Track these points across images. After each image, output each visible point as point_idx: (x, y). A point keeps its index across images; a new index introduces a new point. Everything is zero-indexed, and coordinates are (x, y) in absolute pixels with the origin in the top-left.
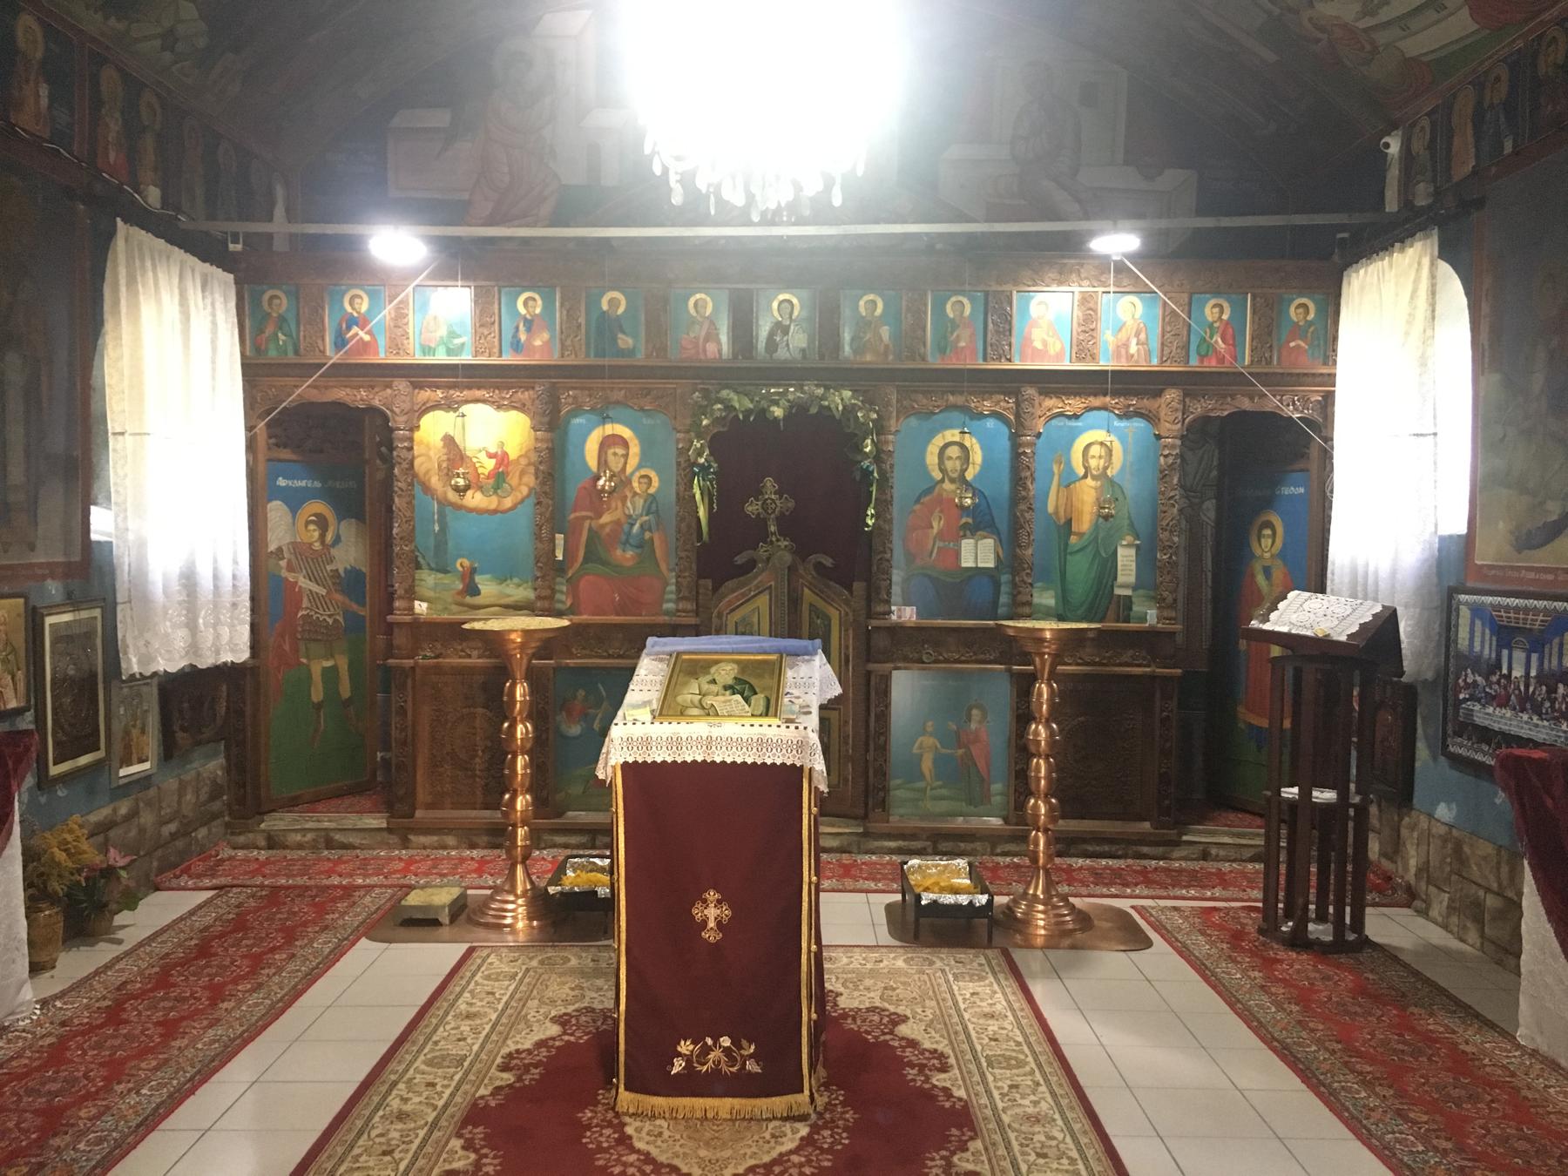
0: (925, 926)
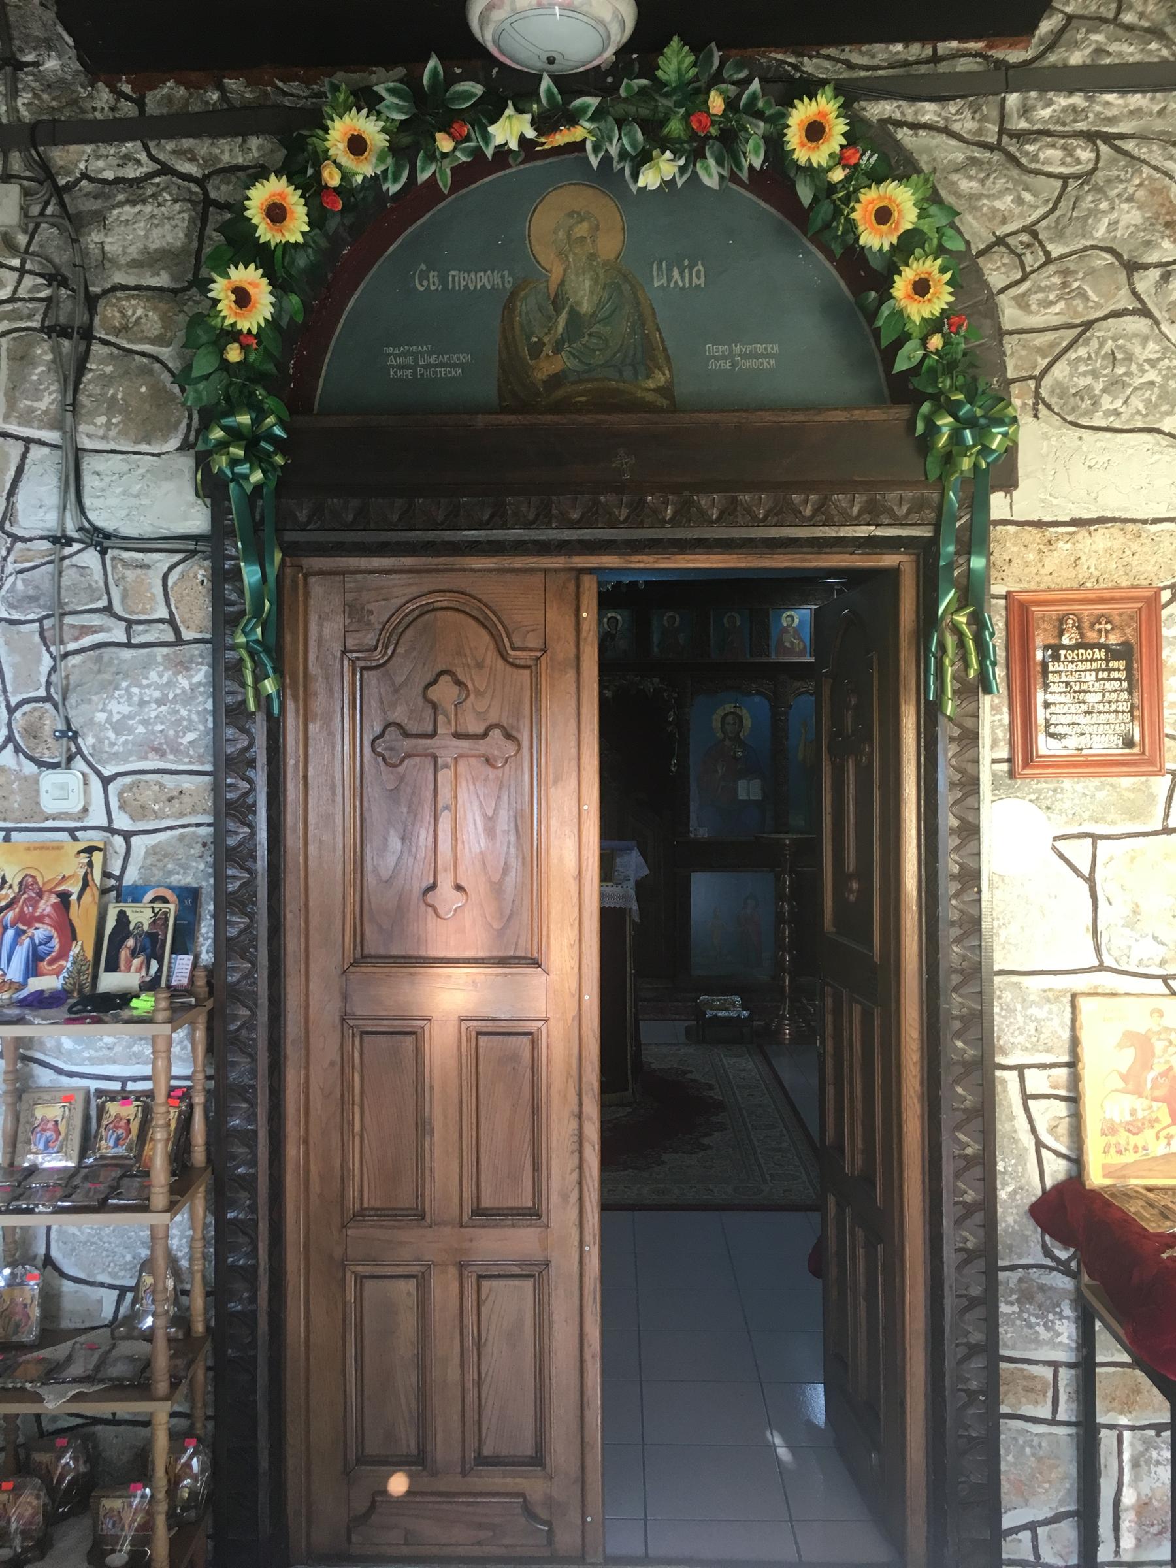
0: (709, 1032)
